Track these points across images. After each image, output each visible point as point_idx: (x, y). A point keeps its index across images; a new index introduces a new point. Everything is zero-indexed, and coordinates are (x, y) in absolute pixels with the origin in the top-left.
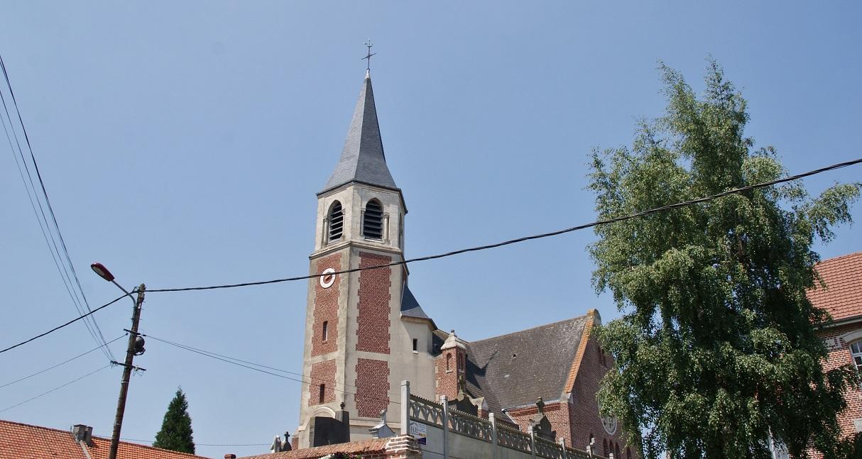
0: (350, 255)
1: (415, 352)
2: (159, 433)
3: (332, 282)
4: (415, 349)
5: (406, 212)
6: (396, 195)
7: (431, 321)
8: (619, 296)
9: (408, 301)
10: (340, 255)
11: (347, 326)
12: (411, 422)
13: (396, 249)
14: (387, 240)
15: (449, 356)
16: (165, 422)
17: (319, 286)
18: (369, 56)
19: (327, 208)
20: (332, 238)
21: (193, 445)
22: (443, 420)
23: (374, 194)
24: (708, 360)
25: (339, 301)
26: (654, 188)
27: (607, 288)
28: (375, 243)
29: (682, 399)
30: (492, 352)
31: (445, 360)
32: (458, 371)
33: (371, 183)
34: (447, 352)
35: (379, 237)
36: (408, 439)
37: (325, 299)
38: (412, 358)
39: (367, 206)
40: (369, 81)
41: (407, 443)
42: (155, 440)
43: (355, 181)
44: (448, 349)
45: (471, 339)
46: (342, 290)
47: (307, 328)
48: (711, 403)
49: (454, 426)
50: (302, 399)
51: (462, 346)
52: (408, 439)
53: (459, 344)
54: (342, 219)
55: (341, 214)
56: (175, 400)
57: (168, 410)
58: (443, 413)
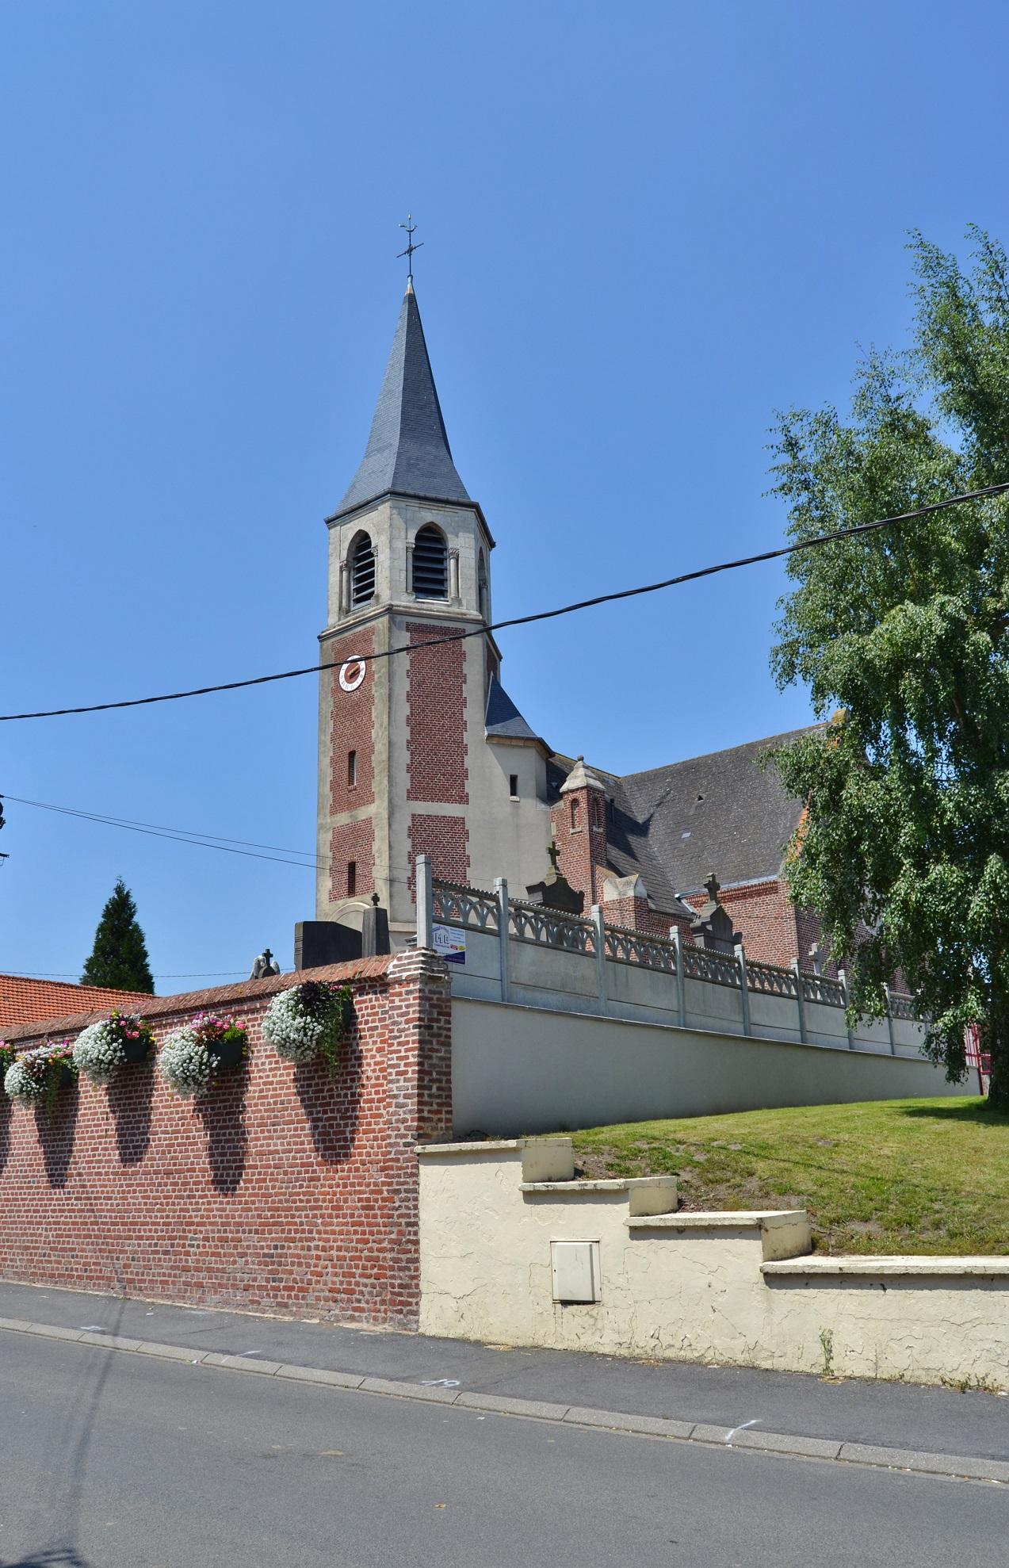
0: (390, 629)
1: (514, 798)
2: (90, 960)
3: (360, 680)
4: (513, 792)
5: (492, 545)
6: (470, 515)
7: (541, 743)
8: (819, 691)
9: (500, 708)
10: (373, 630)
11: (389, 758)
12: (435, 925)
13: (474, 614)
14: (458, 600)
15: (575, 803)
16: (98, 941)
17: (338, 688)
18: (410, 250)
19: (346, 545)
20: (358, 601)
21: (151, 977)
22: (498, 921)
23: (430, 515)
24: (971, 804)
25: (374, 715)
26: (883, 488)
27: (798, 677)
28: (435, 605)
29: (923, 874)
30: (661, 793)
31: (569, 810)
32: (591, 830)
33: (422, 494)
34: (571, 796)
35: (442, 593)
36: (424, 955)
37: (349, 712)
38: (508, 809)
39: (418, 537)
40: (412, 299)
41: (423, 962)
42: (84, 972)
43: (394, 493)
44: (572, 791)
45: (622, 767)
46: (379, 693)
47: (312, 762)
48: (976, 880)
49: (521, 930)
50: (318, 890)
51: (598, 784)
52: (424, 955)
53: (593, 782)
54: (372, 564)
55: (371, 555)
56: (113, 902)
57: (102, 920)
58: (498, 907)
